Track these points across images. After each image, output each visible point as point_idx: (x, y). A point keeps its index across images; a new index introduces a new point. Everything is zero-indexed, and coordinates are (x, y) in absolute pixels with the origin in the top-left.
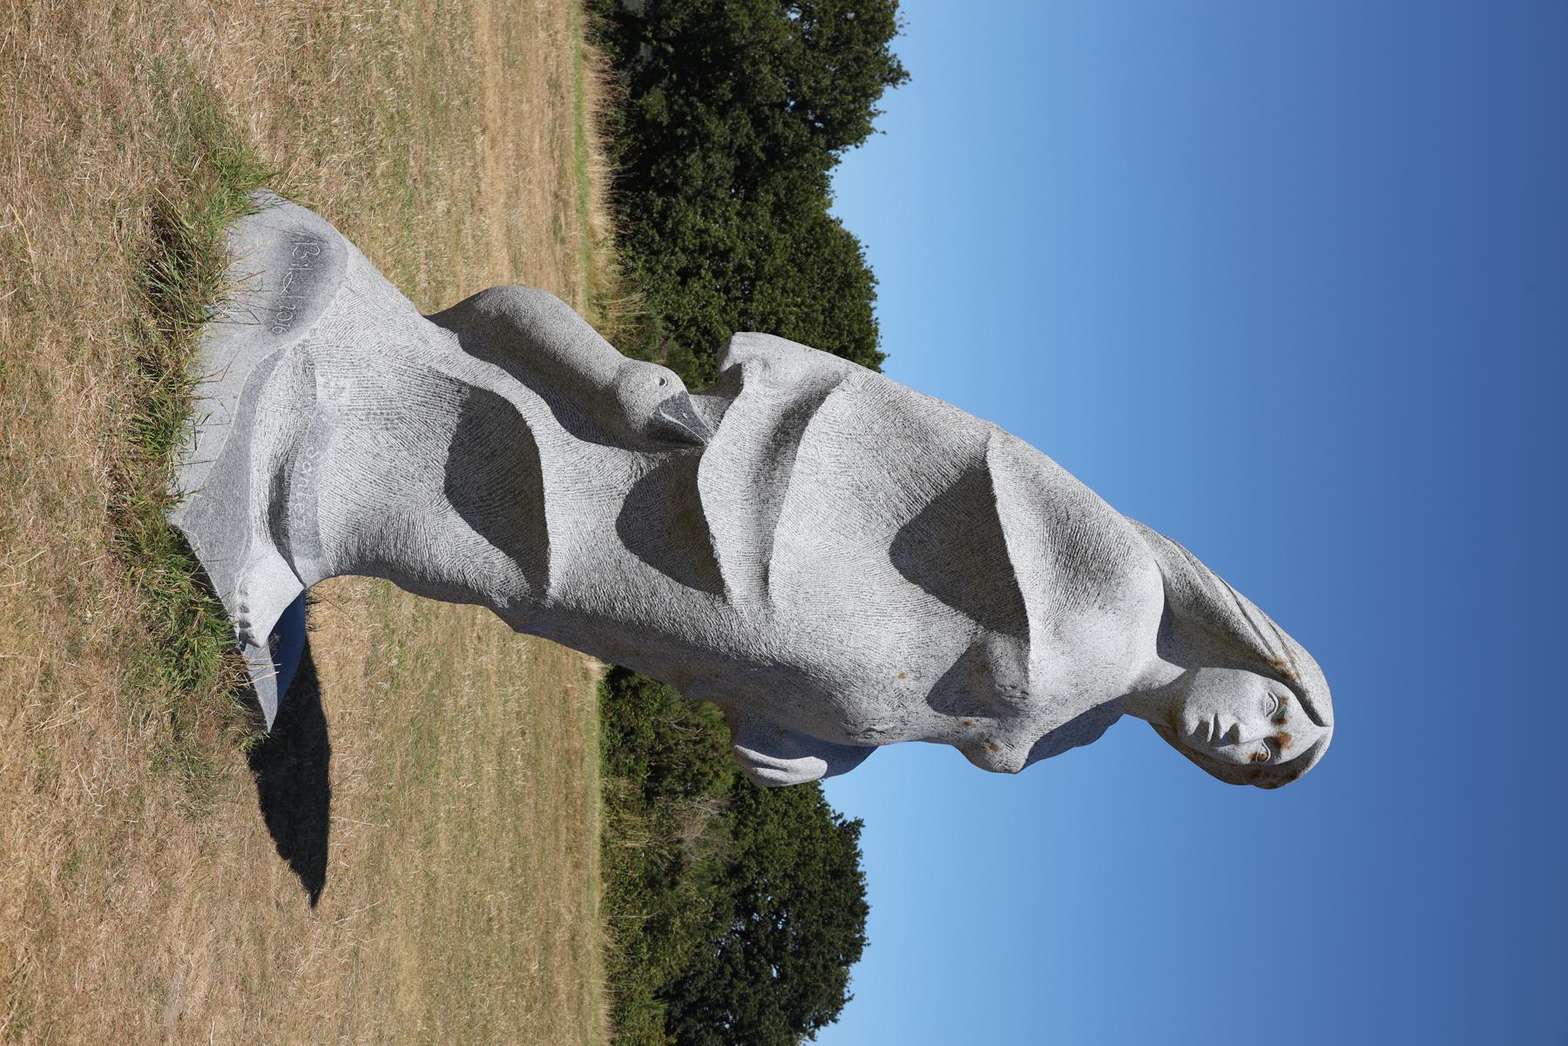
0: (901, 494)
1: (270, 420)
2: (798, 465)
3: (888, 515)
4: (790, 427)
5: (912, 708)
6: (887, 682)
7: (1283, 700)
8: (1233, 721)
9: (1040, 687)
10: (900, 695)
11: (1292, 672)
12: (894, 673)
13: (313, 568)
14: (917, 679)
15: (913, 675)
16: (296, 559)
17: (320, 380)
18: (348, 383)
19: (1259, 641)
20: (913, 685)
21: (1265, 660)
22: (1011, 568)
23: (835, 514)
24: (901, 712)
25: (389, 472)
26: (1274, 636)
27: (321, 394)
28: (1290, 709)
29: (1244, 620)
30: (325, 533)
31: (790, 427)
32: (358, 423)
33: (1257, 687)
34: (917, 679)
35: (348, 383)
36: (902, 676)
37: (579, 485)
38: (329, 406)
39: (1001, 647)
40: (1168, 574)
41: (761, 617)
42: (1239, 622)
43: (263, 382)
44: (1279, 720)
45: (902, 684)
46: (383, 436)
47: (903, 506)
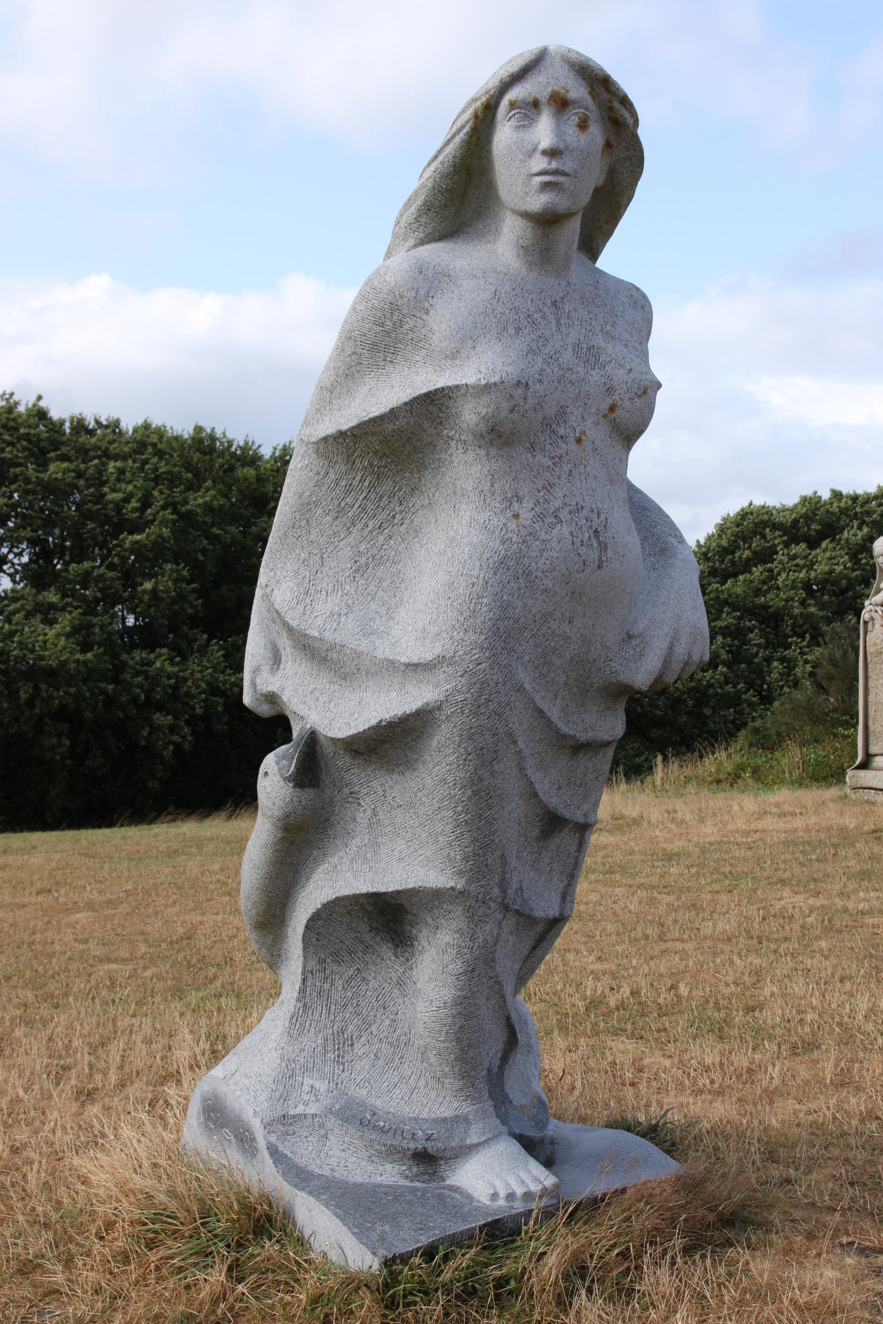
0: (359, 526)
1: (333, 1161)
2: (328, 636)
3: (381, 538)
4: (312, 650)
5: (557, 503)
6: (523, 532)
7: (513, 105)
8: (538, 155)
9: (510, 369)
10: (541, 517)
11: (484, 99)
12: (512, 525)
13: (480, 1125)
14: (520, 500)
15: (516, 505)
16: (468, 1142)
17: (300, 1109)
18: (308, 1082)
19: (458, 139)
20: (528, 504)
21: (474, 130)
22: (392, 410)
23: (380, 593)
24: (564, 514)
25: (391, 1044)
26: (463, 122)
27: (313, 1109)
28: (521, 97)
29: (441, 158)
30: (446, 1112)
31: (312, 650)
32: (347, 1074)
33: (504, 135)
34: (520, 500)
35: (308, 1082)
36: (516, 516)
37: (369, 855)
38: (326, 1101)
39: (470, 414)
40: (411, 242)
41: (450, 670)
42: (442, 163)
43: (295, 1166)
44: (536, 104)
45: (526, 515)
46: (359, 1049)
47: (371, 524)
